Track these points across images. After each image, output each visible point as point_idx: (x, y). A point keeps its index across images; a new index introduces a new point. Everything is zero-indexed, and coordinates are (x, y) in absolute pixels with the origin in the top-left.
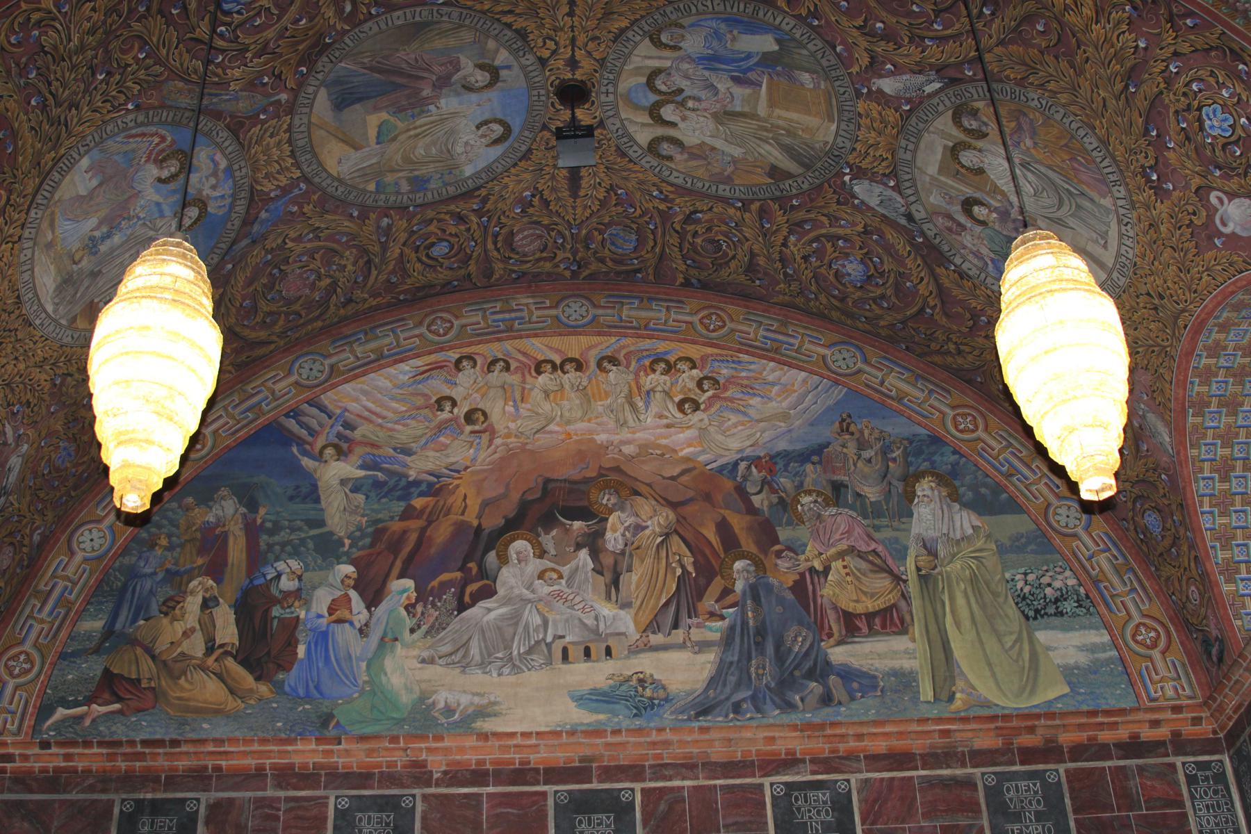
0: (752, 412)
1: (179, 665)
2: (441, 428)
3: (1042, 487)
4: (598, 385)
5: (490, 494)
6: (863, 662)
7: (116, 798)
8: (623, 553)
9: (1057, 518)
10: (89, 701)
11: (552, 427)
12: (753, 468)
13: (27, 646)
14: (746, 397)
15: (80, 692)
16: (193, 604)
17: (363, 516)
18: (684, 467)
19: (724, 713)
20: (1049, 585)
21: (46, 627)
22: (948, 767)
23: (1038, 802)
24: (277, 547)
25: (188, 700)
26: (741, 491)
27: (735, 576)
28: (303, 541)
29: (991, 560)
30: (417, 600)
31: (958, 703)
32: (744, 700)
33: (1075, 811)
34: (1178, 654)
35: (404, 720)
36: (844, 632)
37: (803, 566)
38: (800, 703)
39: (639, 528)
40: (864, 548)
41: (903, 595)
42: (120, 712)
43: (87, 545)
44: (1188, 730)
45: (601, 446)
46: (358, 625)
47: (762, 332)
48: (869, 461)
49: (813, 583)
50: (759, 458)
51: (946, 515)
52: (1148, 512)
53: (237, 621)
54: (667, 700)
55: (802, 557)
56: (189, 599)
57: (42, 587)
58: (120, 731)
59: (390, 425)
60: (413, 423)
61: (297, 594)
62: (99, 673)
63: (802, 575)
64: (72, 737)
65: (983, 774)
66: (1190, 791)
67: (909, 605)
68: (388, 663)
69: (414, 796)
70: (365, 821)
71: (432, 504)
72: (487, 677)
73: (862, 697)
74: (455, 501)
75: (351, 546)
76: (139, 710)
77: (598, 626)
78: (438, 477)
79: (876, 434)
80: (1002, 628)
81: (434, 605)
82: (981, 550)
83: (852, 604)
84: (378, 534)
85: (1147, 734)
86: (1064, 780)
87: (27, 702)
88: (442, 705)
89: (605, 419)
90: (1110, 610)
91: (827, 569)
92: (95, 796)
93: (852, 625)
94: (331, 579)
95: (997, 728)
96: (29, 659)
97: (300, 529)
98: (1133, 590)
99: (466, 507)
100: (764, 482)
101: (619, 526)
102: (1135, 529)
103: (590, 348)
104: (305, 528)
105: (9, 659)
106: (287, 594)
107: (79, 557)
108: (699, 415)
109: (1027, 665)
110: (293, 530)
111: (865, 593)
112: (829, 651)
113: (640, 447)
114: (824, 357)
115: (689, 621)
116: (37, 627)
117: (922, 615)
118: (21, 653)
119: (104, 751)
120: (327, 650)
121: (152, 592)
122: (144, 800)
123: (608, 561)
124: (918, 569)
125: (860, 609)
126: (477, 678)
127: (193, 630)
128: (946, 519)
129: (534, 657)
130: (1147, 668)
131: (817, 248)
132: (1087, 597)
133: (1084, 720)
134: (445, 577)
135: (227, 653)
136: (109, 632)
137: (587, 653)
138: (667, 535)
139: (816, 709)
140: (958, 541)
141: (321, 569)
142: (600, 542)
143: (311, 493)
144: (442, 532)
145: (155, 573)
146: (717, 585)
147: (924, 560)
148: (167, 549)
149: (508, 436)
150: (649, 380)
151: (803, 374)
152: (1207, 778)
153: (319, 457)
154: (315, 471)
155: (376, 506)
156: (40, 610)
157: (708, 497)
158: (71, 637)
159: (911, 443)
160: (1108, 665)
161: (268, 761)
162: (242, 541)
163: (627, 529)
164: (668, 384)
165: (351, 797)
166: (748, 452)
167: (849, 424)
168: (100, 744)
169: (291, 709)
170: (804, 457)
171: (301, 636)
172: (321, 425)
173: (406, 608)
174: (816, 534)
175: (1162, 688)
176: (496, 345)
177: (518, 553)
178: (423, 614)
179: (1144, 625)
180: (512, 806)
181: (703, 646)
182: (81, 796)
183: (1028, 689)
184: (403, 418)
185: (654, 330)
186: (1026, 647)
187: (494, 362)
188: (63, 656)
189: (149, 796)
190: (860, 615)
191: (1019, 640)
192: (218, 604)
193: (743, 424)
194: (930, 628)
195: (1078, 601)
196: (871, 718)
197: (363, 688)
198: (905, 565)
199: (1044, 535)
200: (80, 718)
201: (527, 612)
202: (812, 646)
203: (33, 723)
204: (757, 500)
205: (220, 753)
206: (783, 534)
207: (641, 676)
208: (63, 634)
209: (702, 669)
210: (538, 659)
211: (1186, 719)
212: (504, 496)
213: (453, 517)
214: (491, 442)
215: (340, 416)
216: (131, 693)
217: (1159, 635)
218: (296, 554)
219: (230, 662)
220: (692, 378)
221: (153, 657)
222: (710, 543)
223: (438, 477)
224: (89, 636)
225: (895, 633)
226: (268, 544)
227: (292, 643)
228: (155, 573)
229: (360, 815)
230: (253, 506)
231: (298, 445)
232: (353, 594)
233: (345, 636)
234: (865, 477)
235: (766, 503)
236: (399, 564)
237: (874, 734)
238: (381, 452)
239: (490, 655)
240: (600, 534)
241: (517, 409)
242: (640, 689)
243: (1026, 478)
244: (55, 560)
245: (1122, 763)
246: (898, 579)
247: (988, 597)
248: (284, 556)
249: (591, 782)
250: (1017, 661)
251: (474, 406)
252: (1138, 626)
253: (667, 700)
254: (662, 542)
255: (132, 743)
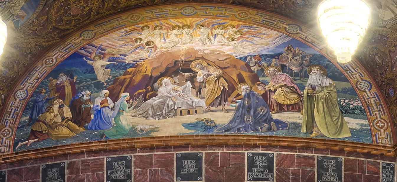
0: (255, 42)
1: (54, 125)
2: (137, 48)
3: (357, 76)
4: (196, 32)
5: (155, 66)
6: (284, 119)
7: (40, 165)
8: (203, 82)
9: (360, 85)
10: (28, 139)
11: (178, 45)
12: (253, 58)
13: (7, 128)
14: (253, 37)
15: (25, 137)
16: (56, 107)
17: (110, 75)
18: (227, 57)
19: (234, 131)
20: (352, 104)
21: (11, 121)
22: (307, 153)
23: (334, 166)
24: (82, 87)
25: (58, 135)
26: (248, 65)
27: (242, 90)
28: (90, 85)
29: (334, 94)
30: (130, 99)
31: (314, 135)
32: (241, 127)
33: (345, 171)
34: (389, 131)
35: (127, 134)
36: (278, 110)
37: (267, 89)
38: (260, 130)
39: (209, 75)
40: (290, 85)
41: (301, 100)
42: (38, 141)
43: (20, 96)
44: (386, 153)
45: (197, 50)
46: (111, 108)
47: (262, 19)
48: (297, 60)
49: (270, 94)
50: (256, 56)
51: (321, 79)
52: (390, 89)
53: (71, 111)
54: (215, 126)
55: (267, 86)
56: (55, 106)
57: (8, 110)
58: (38, 146)
59: (118, 48)
60: (126, 47)
61: (90, 100)
62: (30, 131)
63: (266, 91)
65: (318, 156)
66: (382, 171)
67: (302, 104)
68: (121, 118)
69: (131, 156)
70: (116, 164)
71: (134, 70)
72: (155, 120)
73: (281, 129)
74: (143, 69)
75: (106, 85)
76: (43, 140)
77: (193, 104)
78: (136, 62)
79: (301, 52)
80: (333, 114)
81: (136, 100)
82: (331, 91)
83: (282, 102)
84: (116, 81)
85: (373, 152)
86: (343, 161)
87: (10, 143)
88: (140, 129)
89: (198, 42)
90: (371, 115)
91: (275, 91)
92: (34, 165)
93: (281, 108)
94: (100, 95)
95: (324, 143)
96: (8, 131)
97: (89, 81)
98: (380, 111)
99: (146, 70)
100: (256, 63)
101: (202, 74)
102: (385, 93)
103: (194, 22)
104: (91, 81)
105: (2, 132)
106: (87, 101)
107: (18, 100)
108: (234, 42)
109: (339, 126)
110: (86, 82)
111: (288, 99)
112: (272, 115)
113: (211, 51)
114: (285, 28)
115: (225, 103)
116: (9, 122)
117: (306, 107)
118: (6, 130)
119: (34, 152)
120: (101, 116)
121: (43, 106)
122: (48, 164)
123: (197, 85)
124: (308, 93)
125: (285, 103)
126: (151, 120)
127: (57, 115)
128: (321, 80)
129: (170, 114)
130: (378, 133)
132: (364, 110)
133: (353, 145)
134: (140, 91)
135: (68, 120)
136: (31, 119)
137: (189, 112)
138: (219, 77)
139: (266, 132)
140: (323, 87)
141: (97, 92)
142: (195, 79)
143: (91, 70)
144: (138, 78)
145: (43, 101)
146: (234, 94)
147: (310, 91)
148: (45, 93)
149: (162, 48)
150: (215, 32)
151: (276, 32)
152: (388, 168)
153: (93, 60)
154: (92, 64)
155: (114, 72)
156: (9, 117)
157: (235, 66)
158: (20, 123)
159: (313, 56)
160: (366, 131)
161: (84, 150)
162: (70, 87)
163: (205, 75)
164: (223, 32)
165: (111, 158)
166: (252, 54)
167: (291, 48)
168: (33, 151)
169: (90, 134)
170: (272, 56)
171: (92, 113)
172: (93, 50)
173: (127, 101)
174: (273, 80)
175: (381, 140)
176: (157, 22)
177: (165, 83)
178: (132, 102)
179: (381, 121)
180: (162, 158)
181: (228, 111)
182: (30, 166)
183: (338, 133)
184: (123, 45)
185: (219, 16)
186: (340, 121)
187: (157, 27)
188: (18, 128)
189: (50, 163)
190: (285, 105)
191: (338, 119)
192: (64, 106)
193: (251, 45)
194: (308, 112)
195: (360, 111)
196: (284, 136)
197: (113, 126)
198: (303, 92)
199: (354, 90)
200: (27, 144)
201: (168, 100)
202: (267, 113)
203: (13, 148)
204: (253, 68)
205: (69, 149)
206: (261, 79)
207: (207, 119)
208: (17, 122)
209: (228, 118)
210: (172, 114)
211: (386, 150)
212: (160, 66)
213: (142, 73)
214: (155, 50)
215: (100, 47)
216: (40, 135)
217: (384, 125)
218: (88, 88)
219: (70, 123)
220: (233, 31)
221: (46, 124)
222: (234, 80)
223: (136, 62)
224: (25, 121)
225: (296, 112)
226: (78, 87)
227: (89, 115)
228: (43, 101)
229: (114, 162)
230: (72, 77)
231: (85, 57)
232: (108, 99)
234: (294, 64)
235: (256, 69)
236: (123, 88)
237: (283, 141)
238: (115, 56)
239: (155, 114)
240: (195, 77)
241: (165, 40)
242: (206, 123)
243: (352, 72)
244: (11, 102)
245: (363, 159)
246: (300, 95)
247: (330, 104)
248: (84, 90)
249: (189, 151)
250: (336, 125)
251: (149, 40)
252: (379, 121)
253: (215, 126)
254: (217, 79)
255: (42, 149)
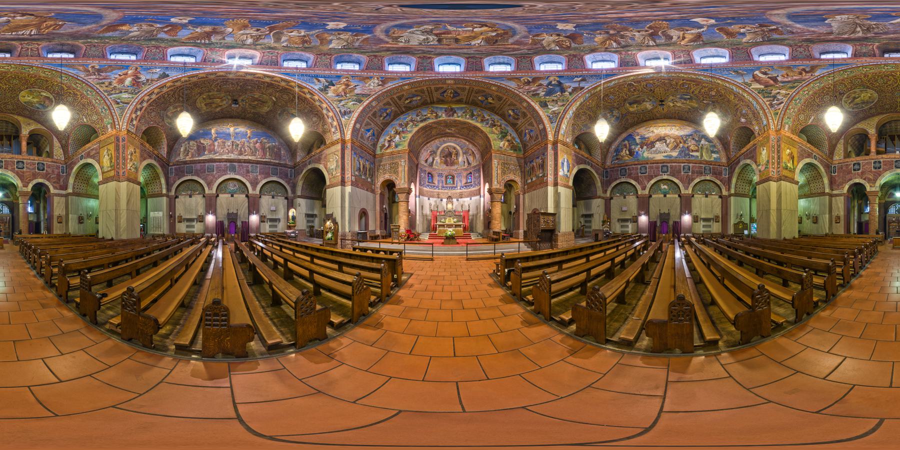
64: (615, 164)
93: (693, 151)
131: (732, 331)
143: (635, 139)
144: (649, 142)
233: (640, 152)
